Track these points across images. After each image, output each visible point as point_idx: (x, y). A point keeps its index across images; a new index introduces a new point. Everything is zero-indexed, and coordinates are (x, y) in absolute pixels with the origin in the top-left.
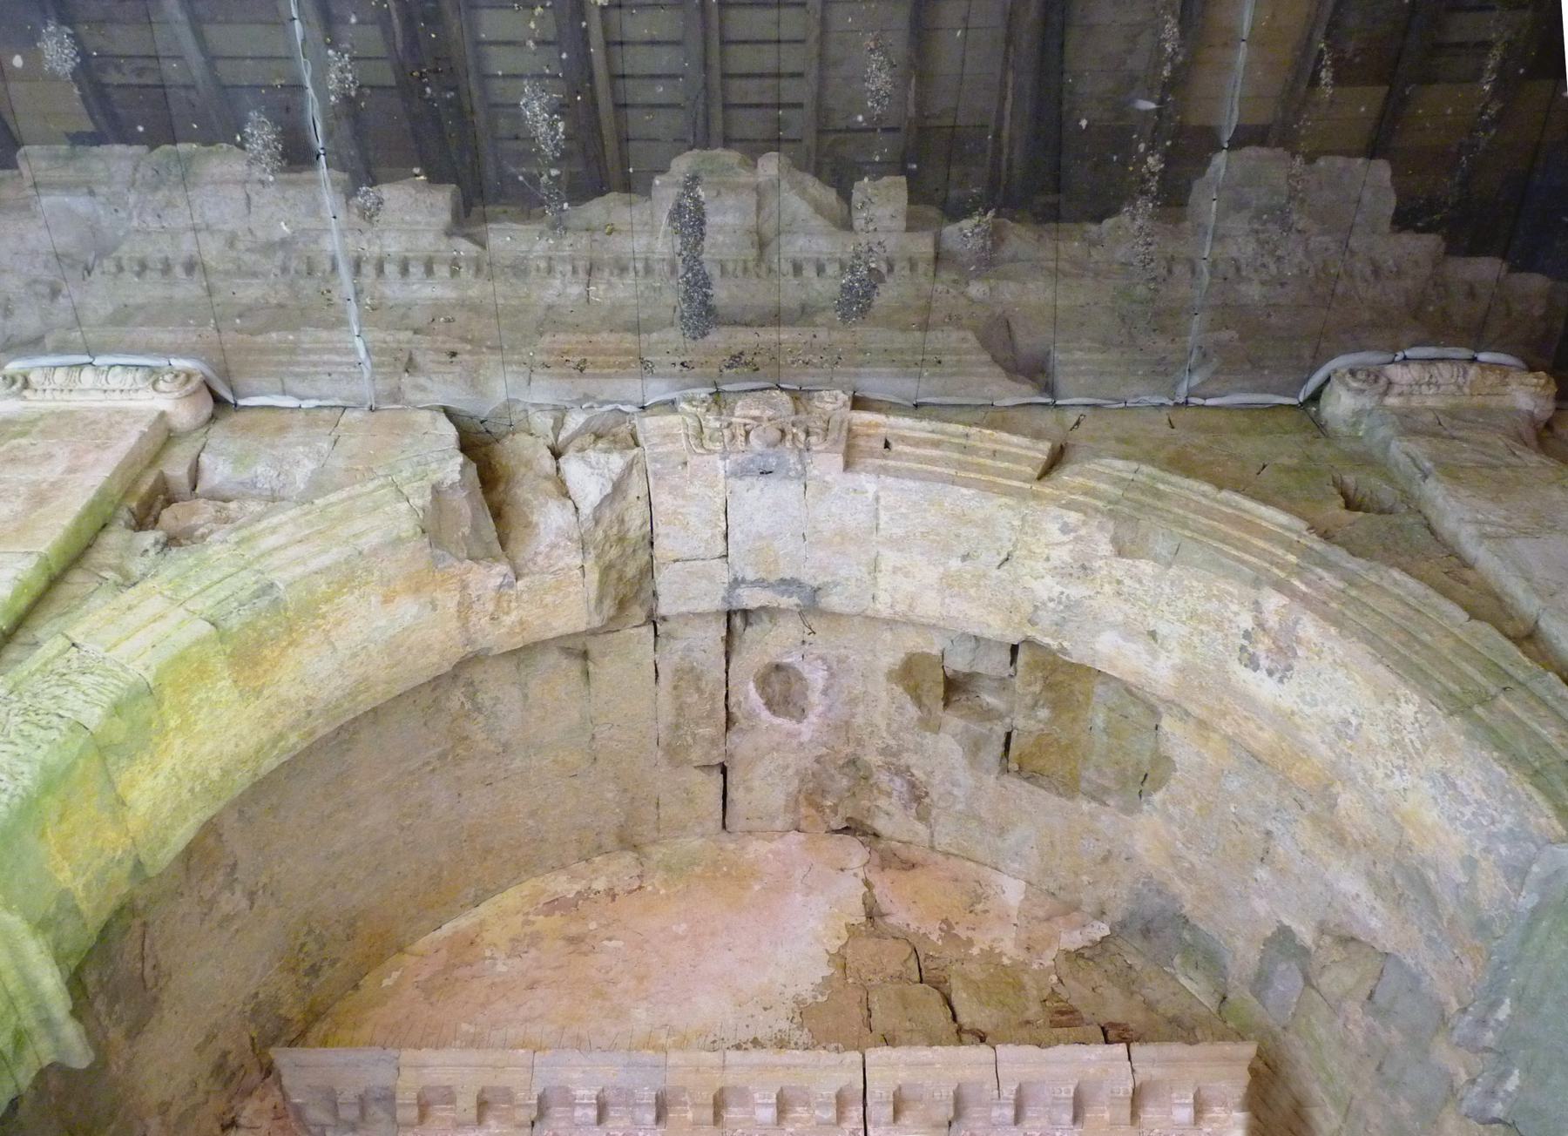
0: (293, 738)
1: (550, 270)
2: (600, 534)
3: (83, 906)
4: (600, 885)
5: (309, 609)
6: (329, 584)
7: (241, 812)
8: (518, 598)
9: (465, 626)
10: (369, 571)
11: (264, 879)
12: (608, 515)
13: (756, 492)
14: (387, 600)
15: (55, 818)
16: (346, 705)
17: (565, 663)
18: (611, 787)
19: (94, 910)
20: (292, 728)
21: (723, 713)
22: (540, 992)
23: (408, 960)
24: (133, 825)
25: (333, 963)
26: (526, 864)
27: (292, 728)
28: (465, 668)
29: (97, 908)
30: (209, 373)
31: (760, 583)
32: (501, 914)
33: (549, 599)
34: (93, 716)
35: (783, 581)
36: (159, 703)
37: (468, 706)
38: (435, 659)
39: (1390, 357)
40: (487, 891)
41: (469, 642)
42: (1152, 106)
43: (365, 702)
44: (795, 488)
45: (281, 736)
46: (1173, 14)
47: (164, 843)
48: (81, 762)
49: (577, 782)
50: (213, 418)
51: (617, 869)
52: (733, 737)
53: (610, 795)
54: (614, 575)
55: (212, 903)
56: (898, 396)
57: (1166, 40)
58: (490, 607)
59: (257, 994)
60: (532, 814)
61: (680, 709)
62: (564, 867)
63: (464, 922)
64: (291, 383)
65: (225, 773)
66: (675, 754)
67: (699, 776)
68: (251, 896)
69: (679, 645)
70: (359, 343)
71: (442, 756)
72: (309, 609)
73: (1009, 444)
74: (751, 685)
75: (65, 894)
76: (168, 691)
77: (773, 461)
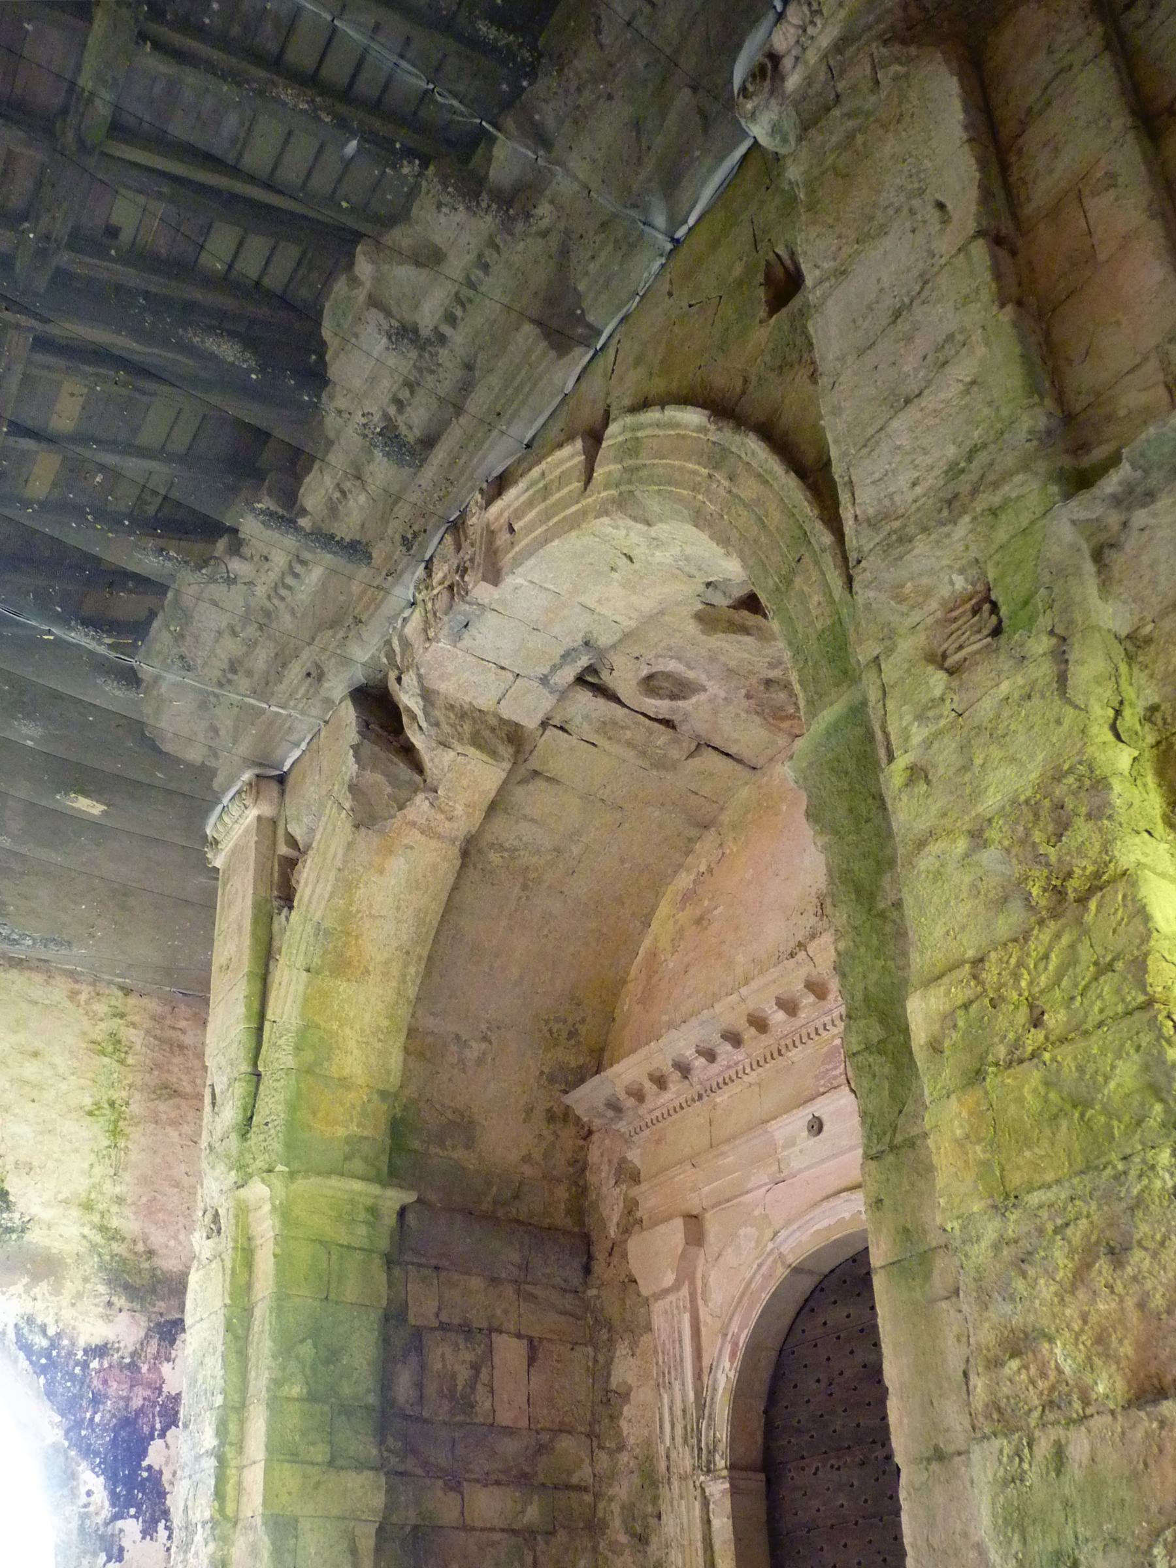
0: (412, 970)
1: (343, 493)
2: (446, 728)
3: (366, 1134)
4: (703, 869)
5: (346, 917)
6: (342, 898)
7: (432, 1014)
8: (449, 798)
9: (439, 837)
10: (356, 871)
11: (484, 1027)
12: (438, 714)
13: (478, 636)
14: (381, 872)
15: (311, 1117)
16: (424, 930)
17: (531, 787)
18: (650, 809)
19: (375, 1130)
20: (405, 966)
21: (656, 725)
22: (692, 971)
23: (630, 986)
24: (361, 1081)
25: (583, 1021)
26: (657, 883)
27: (405, 966)
28: (469, 851)
29: (375, 1127)
30: (257, 771)
31: (555, 668)
32: (660, 929)
33: (465, 783)
34: (290, 1061)
35: (563, 657)
36: (318, 1027)
37: (506, 854)
38: (446, 865)
39: (771, 17)
40: (645, 916)
41: (453, 841)
42: (354, 143)
43: (434, 920)
44: (490, 615)
45: (404, 976)
46: (275, 85)
47: (388, 1072)
48: (302, 1085)
49: (626, 826)
50: (282, 793)
51: (707, 845)
52: (683, 728)
53: (657, 814)
54: (486, 733)
55: (462, 1061)
56: (512, 455)
57: (296, 105)
58: (441, 817)
59: (542, 1073)
60: (622, 861)
61: (629, 744)
62: (681, 866)
63: (647, 943)
64: (294, 737)
65: (390, 1017)
66: (662, 764)
67: (695, 762)
68: (485, 1039)
69: (578, 720)
70: (274, 709)
71: (525, 887)
72: (346, 917)
73: (561, 462)
74: (648, 700)
75: (348, 1140)
76: (316, 1018)
77: (460, 618)
